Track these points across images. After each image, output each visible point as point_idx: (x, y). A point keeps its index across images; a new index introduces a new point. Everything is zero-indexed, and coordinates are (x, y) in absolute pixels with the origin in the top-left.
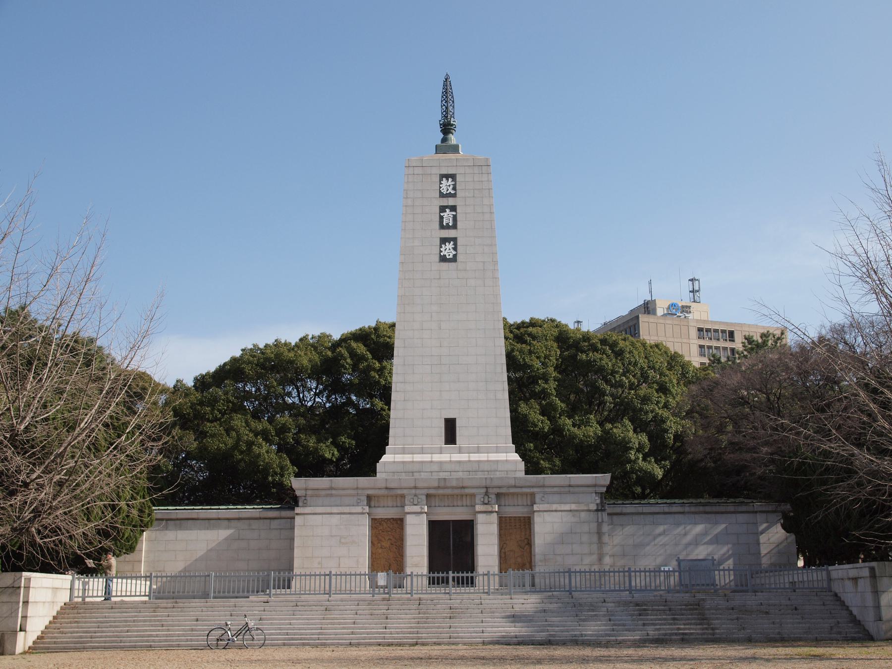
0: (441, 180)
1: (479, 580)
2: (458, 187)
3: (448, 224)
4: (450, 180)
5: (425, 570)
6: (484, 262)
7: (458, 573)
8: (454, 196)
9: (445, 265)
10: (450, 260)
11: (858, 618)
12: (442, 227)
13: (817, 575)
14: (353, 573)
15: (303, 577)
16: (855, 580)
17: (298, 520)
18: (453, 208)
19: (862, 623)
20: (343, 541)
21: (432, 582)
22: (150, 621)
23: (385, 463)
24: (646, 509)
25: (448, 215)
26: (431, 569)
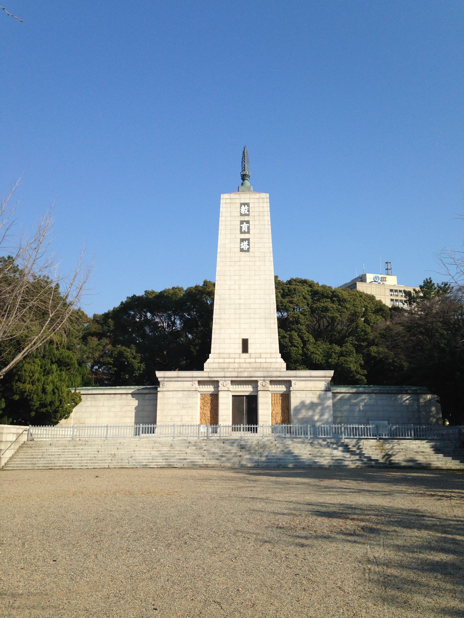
0: (241, 206)
2: (250, 210)
3: (244, 231)
4: (246, 206)
5: (231, 423)
6: (265, 252)
8: (248, 215)
9: (243, 254)
12: (241, 232)
14: (190, 425)
15: (97, 428)
17: (159, 395)
18: (248, 222)
20: (184, 406)
23: (208, 363)
25: (245, 226)
26: (234, 422)
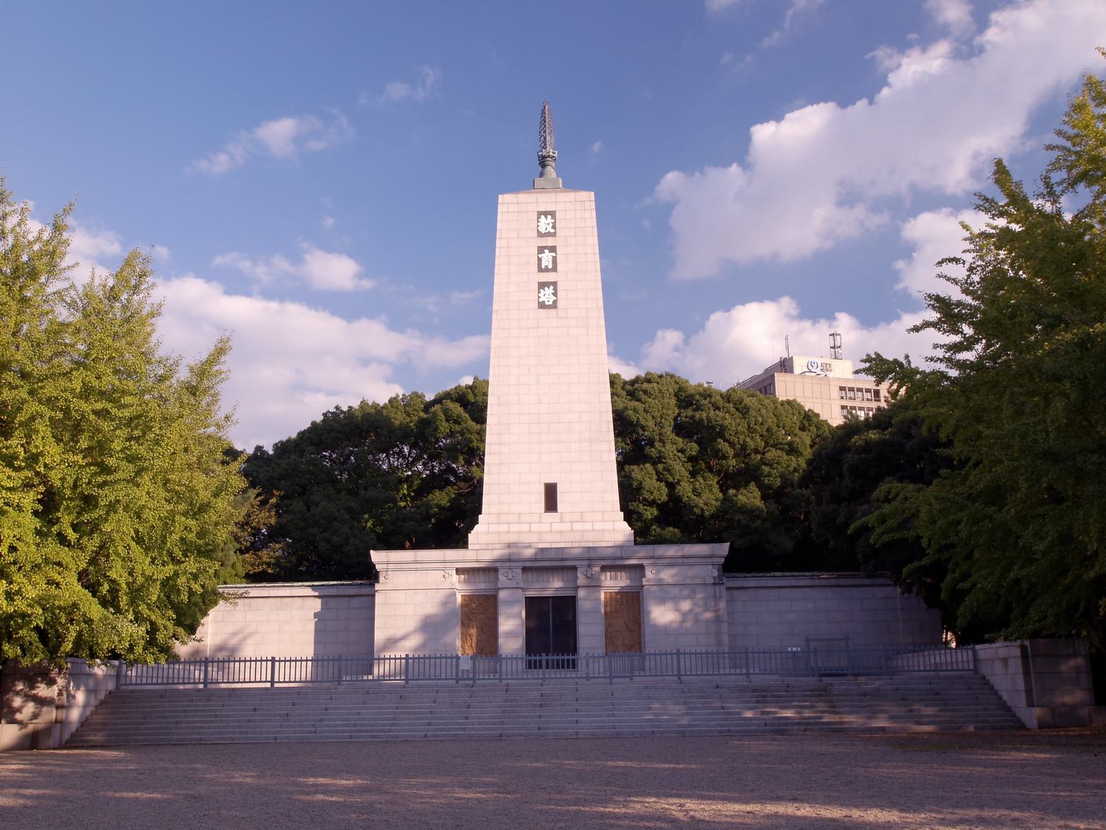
0: (539, 217)
1: (581, 663)
3: (546, 267)
4: (549, 217)
7: (558, 655)
8: (554, 235)
9: (544, 312)
10: (549, 307)
11: (1009, 703)
12: (540, 270)
13: (965, 655)
16: (1005, 661)
19: (1014, 709)
21: (531, 665)
22: (408, 713)
24: (771, 582)
25: (547, 258)
